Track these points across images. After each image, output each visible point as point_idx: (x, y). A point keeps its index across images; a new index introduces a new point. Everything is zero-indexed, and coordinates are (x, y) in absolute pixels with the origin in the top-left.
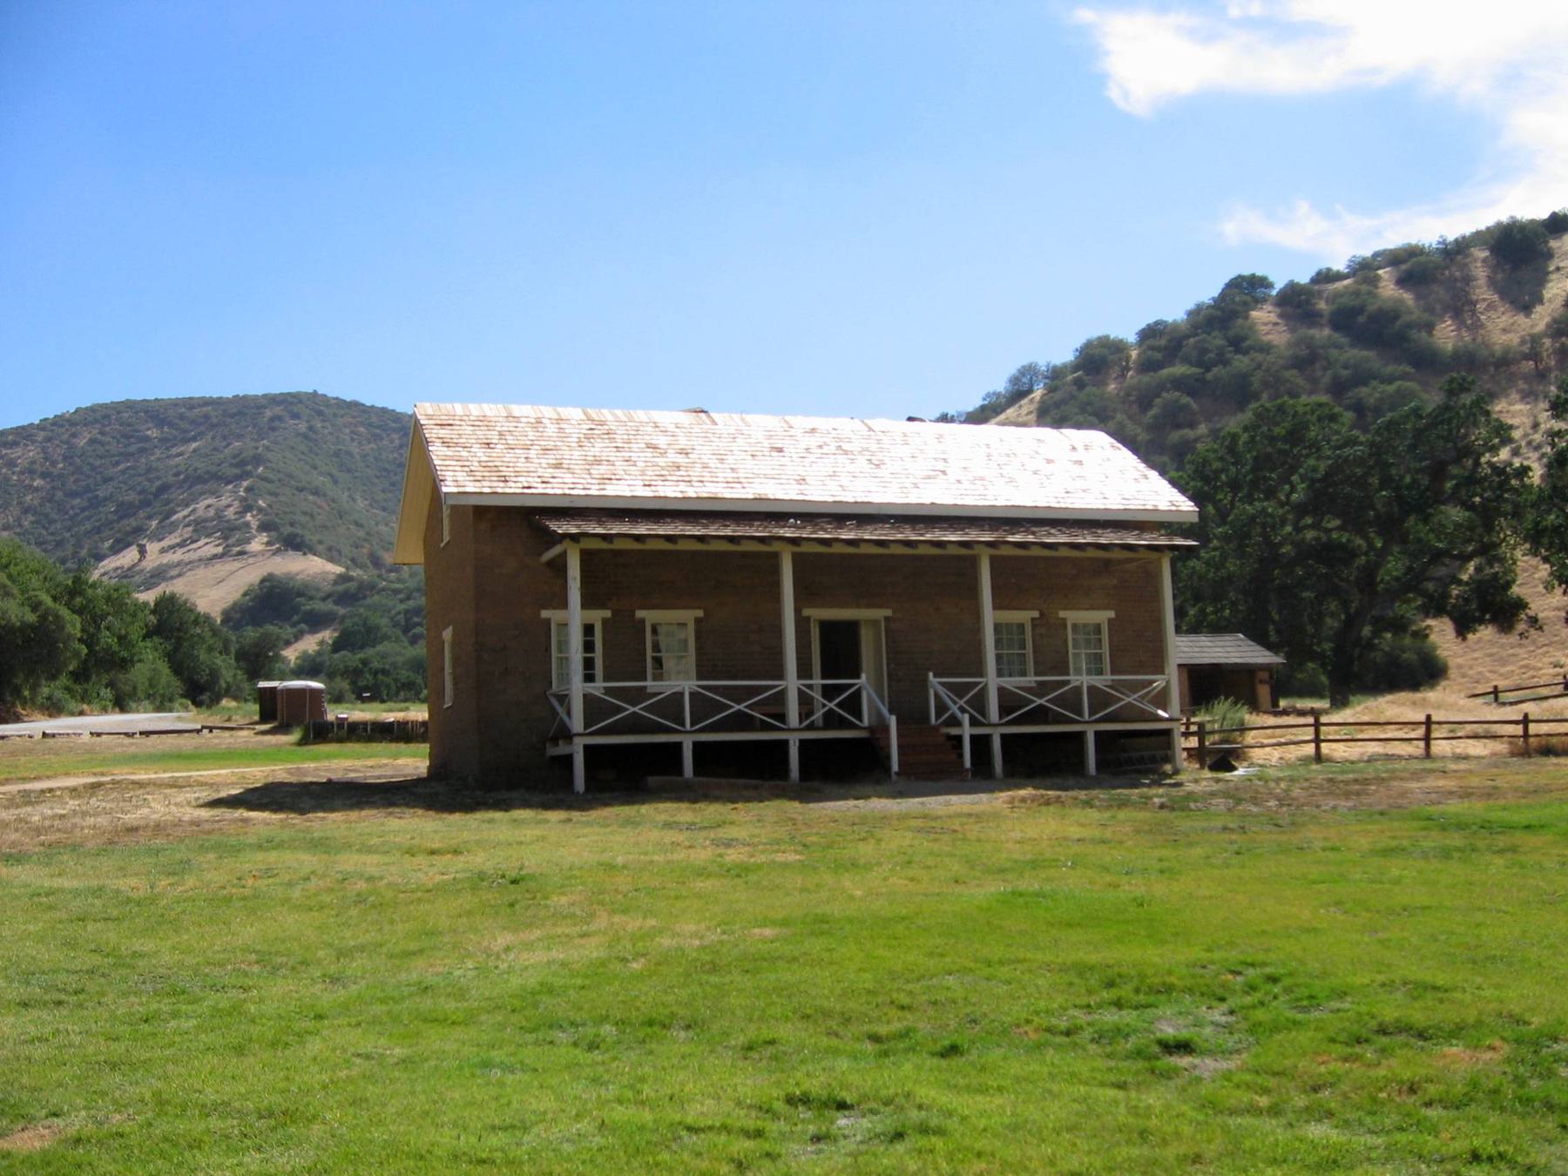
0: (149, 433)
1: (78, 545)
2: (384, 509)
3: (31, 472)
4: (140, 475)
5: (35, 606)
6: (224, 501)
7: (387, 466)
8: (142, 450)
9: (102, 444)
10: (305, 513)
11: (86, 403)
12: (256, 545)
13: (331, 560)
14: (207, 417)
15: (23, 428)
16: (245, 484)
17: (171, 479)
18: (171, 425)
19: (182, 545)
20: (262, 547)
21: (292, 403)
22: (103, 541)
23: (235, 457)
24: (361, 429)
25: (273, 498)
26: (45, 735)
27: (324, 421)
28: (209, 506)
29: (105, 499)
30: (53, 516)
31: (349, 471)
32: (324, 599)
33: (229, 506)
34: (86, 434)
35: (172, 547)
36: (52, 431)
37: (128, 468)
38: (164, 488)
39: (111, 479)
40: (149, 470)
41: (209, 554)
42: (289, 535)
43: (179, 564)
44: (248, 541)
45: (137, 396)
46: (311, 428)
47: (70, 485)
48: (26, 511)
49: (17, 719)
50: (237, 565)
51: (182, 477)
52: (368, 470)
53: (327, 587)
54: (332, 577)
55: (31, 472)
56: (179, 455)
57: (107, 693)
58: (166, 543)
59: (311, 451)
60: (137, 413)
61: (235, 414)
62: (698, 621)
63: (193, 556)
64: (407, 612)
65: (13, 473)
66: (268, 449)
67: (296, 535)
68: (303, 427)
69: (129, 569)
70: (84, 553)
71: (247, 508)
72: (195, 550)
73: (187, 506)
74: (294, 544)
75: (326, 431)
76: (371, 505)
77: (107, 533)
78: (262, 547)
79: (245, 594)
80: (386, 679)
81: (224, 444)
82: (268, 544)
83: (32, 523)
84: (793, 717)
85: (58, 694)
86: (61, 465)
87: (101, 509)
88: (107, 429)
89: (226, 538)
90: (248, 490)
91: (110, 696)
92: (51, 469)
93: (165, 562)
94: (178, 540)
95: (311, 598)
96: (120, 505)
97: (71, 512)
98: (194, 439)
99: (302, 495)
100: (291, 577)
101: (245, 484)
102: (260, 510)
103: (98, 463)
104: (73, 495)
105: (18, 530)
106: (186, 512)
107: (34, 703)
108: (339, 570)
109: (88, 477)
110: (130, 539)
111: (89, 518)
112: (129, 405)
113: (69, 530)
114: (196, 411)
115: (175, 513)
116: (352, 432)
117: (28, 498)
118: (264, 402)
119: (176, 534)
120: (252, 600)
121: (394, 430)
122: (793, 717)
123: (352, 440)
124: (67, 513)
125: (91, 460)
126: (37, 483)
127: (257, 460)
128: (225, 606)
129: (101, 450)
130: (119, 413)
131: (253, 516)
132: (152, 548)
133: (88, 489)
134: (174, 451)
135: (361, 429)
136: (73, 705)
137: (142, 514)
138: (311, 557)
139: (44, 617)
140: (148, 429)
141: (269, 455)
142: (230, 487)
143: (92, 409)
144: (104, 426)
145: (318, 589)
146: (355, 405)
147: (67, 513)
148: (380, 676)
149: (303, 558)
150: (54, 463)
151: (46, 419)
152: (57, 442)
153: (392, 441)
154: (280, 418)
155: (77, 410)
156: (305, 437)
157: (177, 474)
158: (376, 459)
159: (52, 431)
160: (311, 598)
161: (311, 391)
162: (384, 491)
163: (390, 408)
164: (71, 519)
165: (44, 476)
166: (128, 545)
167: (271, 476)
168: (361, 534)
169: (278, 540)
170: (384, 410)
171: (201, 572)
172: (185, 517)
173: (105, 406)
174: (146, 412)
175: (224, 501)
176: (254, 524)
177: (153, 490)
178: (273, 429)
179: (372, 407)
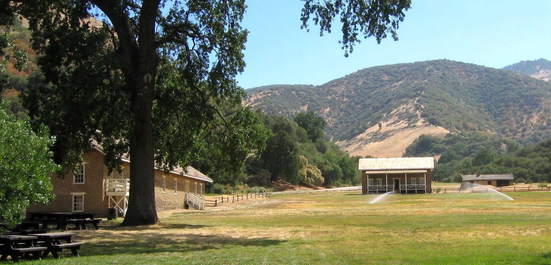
0: (384, 78)
1: (359, 124)
2: (471, 105)
3: (343, 96)
4: (381, 95)
5: (333, 167)
6: (409, 106)
7: (472, 87)
8: (381, 86)
9: (367, 84)
10: (438, 109)
11: (361, 68)
12: (419, 123)
13: (446, 128)
14: (404, 71)
15: (339, 79)
16: (417, 99)
17: (391, 97)
18: (392, 75)
19: (394, 123)
20: (421, 124)
21: (436, 64)
22: (367, 122)
23: (414, 88)
24: (463, 73)
25: (427, 104)
26: (333, 191)
27: (448, 71)
28: (403, 108)
29: (369, 105)
30: (351, 112)
31: (458, 90)
32: (441, 143)
33: (411, 108)
34: (361, 80)
35: (390, 124)
36: (349, 80)
37: (377, 93)
38: (389, 100)
39: (370, 97)
40: (384, 93)
41: (403, 127)
42: (431, 119)
43: (392, 131)
44: (417, 121)
45: (379, 64)
46: (443, 74)
47: (356, 100)
48: (341, 110)
49: (331, 188)
50: (412, 131)
51: (395, 96)
52: (465, 89)
53: (443, 139)
54: (445, 135)
55: (343, 96)
56: (394, 87)
57: (350, 182)
58: (388, 123)
59: (443, 83)
60: (379, 71)
61: (416, 70)
62: (382, 180)
63: (397, 128)
64: (469, 147)
65: (337, 96)
66: (426, 84)
67: (434, 119)
68: (440, 74)
69: (376, 133)
70: (361, 126)
71: (417, 109)
72: (398, 125)
73: (396, 108)
74: (434, 122)
75: (449, 75)
76: (466, 103)
77: (369, 118)
78: (421, 124)
79: (414, 142)
80: (442, 174)
81: (411, 81)
82: (424, 122)
83: (344, 115)
84: (406, 188)
85: (339, 183)
86: (353, 93)
87: (367, 109)
88: (369, 78)
89: (409, 120)
90: (418, 101)
91: (351, 183)
92: (349, 94)
93: (388, 130)
94: (393, 121)
95: (437, 143)
96: (374, 108)
97: (357, 110)
98: (400, 80)
99: (438, 102)
100: (429, 135)
101: (417, 99)
102: (422, 109)
103: (366, 91)
104: (357, 104)
105: (338, 118)
106: (395, 111)
107: (334, 184)
108: (448, 132)
109: (362, 97)
110: (376, 121)
111: (363, 112)
112: (376, 68)
113: (356, 117)
114: (401, 69)
115: (392, 111)
116: (459, 74)
117: (342, 106)
118: (425, 64)
119: (392, 119)
120: (416, 144)
121: (476, 72)
122: (406, 188)
123: (460, 77)
124: (355, 111)
125: (363, 90)
126: (345, 100)
127: (422, 89)
128: (407, 146)
129: (367, 86)
130: (373, 71)
131: (419, 112)
132: (384, 124)
133: (362, 101)
134: (393, 85)
135: (463, 73)
136: (342, 185)
137: (381, 111)
138: (438, 127)
139: (335, 169)
140: (384, 77)
141: (426, 86)
142: (412, 100)
143: (363, 71)
144: (368, 77)
145: (439, 140)
146: (461, 63)
147: (355, 111)
148: (440, 174)
149: (436, 128)
150: (351, 92)
151: (347, 76)
152: (351, 84)
153: (475, 77)
154: (432, 71)
155: (358, 71)
156: (441, 78)
157: (393, 95)
158: (468, 84)
159: (349, 80)
160: (437, 143)
161: (443, 59)
162: (471, 97)
163: (474, 63)
164: (357, 112)
165: (347, 97)
166: (376, 123)
167: (427, 95)
168: (460, 116)
169: (427, 121)
170: (472, 65)
171: (400, 134)
172: (395, 112)
173: (368, 69)
174: (383, 70)
175: (409, 106)
176: (419, 115)
177: (385, 101)
178: (429, 75)
179: (467, 64)
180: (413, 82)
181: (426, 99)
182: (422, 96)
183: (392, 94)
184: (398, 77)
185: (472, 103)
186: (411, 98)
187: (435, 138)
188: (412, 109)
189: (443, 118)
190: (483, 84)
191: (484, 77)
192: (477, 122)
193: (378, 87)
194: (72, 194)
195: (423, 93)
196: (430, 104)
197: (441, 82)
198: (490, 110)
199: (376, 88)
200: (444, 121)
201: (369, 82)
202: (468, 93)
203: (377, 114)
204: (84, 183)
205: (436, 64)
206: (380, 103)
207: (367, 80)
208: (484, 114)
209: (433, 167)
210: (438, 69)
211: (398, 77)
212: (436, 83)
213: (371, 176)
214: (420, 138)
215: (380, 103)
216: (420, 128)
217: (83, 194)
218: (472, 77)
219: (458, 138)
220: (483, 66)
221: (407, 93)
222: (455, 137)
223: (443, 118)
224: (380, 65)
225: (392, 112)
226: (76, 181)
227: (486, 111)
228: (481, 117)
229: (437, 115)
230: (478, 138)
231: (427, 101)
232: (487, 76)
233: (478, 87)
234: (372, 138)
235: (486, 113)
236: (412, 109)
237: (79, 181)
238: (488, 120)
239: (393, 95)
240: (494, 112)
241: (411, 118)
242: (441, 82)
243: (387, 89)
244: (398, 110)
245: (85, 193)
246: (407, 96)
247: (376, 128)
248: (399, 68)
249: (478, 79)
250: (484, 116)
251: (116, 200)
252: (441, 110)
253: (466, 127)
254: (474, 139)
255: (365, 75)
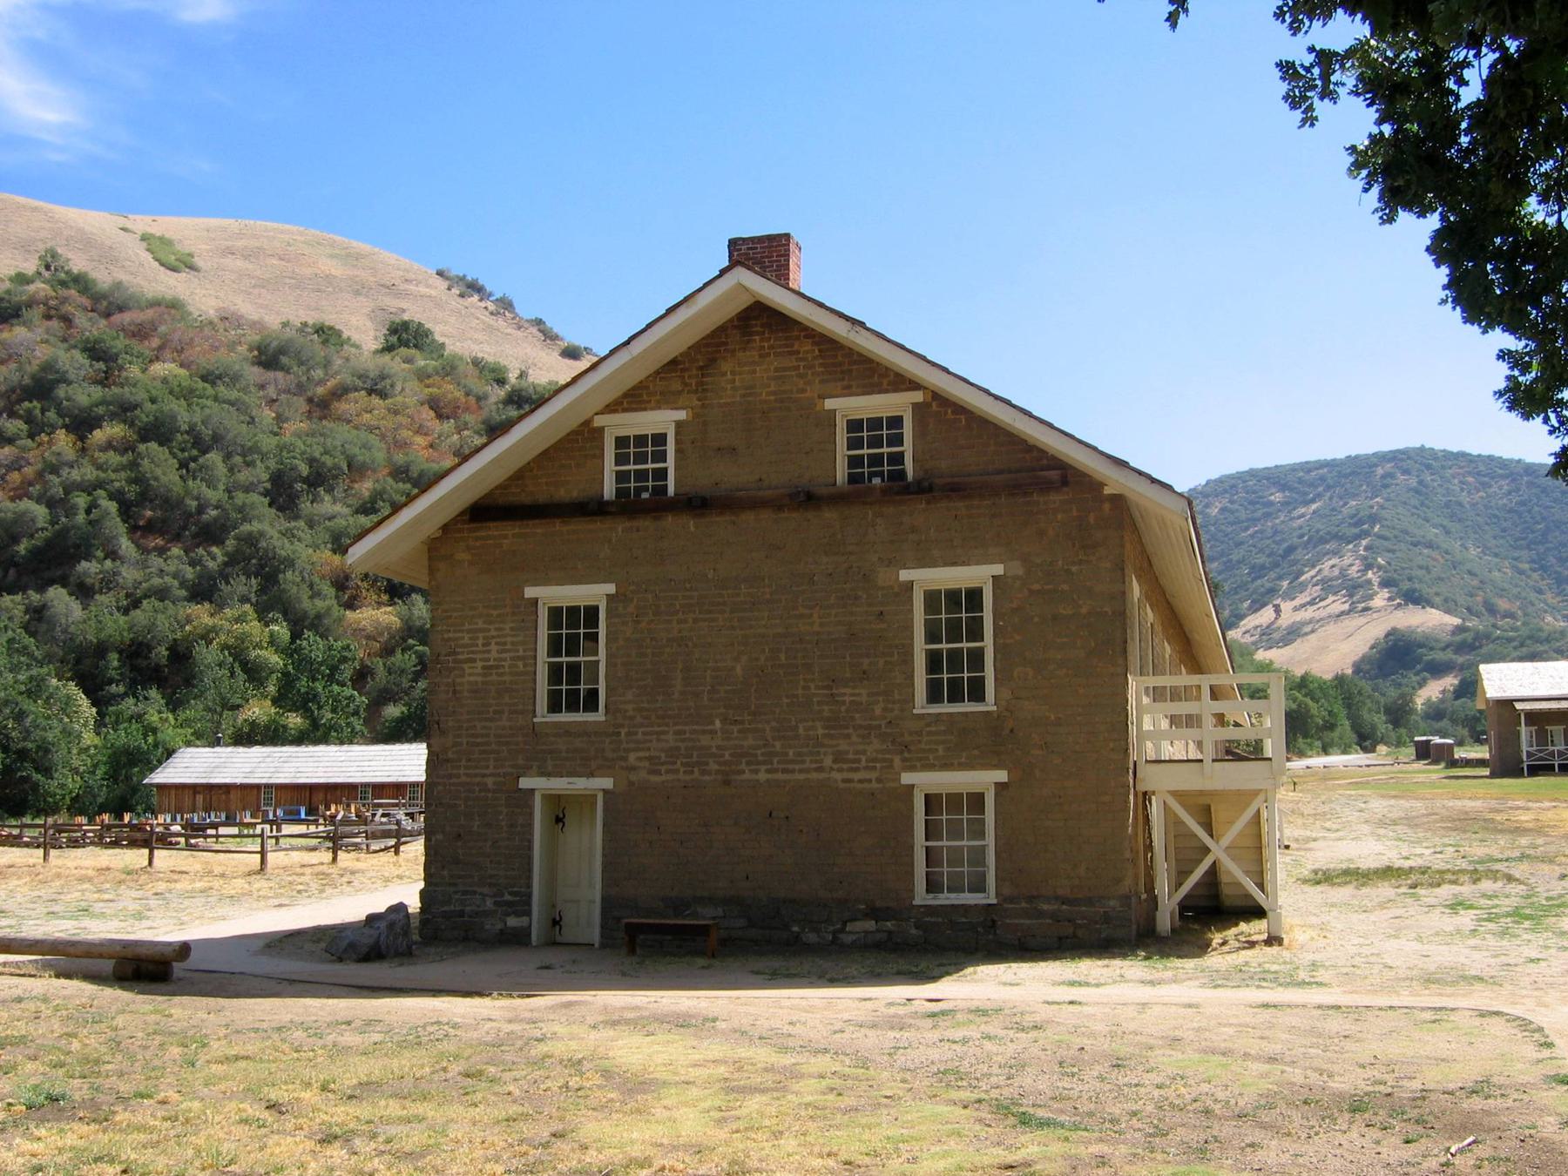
2: (1496, 555)
6: (1347, 561)
7: (1496, 512)
8: (1267, 515)
9: (1232, 512)
10: (1421, 567)
11: (1215, 476)
12: (1379, 601)
13: (1448, 612)
14: (1322, 479)
16: (1364, 543)
18: (1291, 489)
19: (1312, 603)
20: (1384, 603)
21: (1402, 460)
23: (1352, 518)
24: (1470, 479)
25: (1390, 555)
27: (1432, 474)
28: (1333, 566)
29: (1239, 562)
32: (1444, 649)
33: (1351, 565)
35: (1303, 606)
37: (1256, 532)
38: (1291, 549)
39: (1241, 543)
40: (1276, 532)
42: (1408, 590)
43: (1311, 621)
44: (1371, 597)
46: (1421, 482)
50: (1363, 620)
54: (1450, 628)
58: (1297, 602)
59: (1422, 504)
61: (1350, 474)
63: (1323, 613)
66: (1382, 507)
67: (1414, 591)
68: (1413, 482)
69: (1268, 627)
71: (1369, 567)
73: (1313, 566)
74: (1413, 598)
76: (1483, 552)
78: (1384, 603)
79: (1372, 647)
82: (1390, 599)
89: (1351, 596)
90: (1367, 548)
95: (1432, 649)
96: (1253, 567)
98: (1313, 501)
99: (1416, 550)
101: (1364, 543)
102: (1380, 567)
103: (1230, 530)
106: (1313, 573)
108: (1457, 621)
112: (1252, 473)
115: (1303, 574)
116: (1461, 482)
119: (1306, 593)
120: (1379, 652)
121: (1502, 477)
123: (1462, 490)
127: (1373, 519)
128: (1356, 657)
129: (1231, 518)
132: (1286, 606)
133: (1222, 554)
134: (1296, 513)
135: (1470, 479)
137: (1273, 575)
138: (1428, 609)
139: (1299, 706)
142: (1351, 546)
143: (1220, 481)
145: (1437, 641)
146: (1463, 455)
153: (1500, 488)
154: (1391, 475)
155: (1208, 482)
157: (1301, 536)
160: (1432, 649)
161: (1418, 445)
162: (1495, 538)
170: (1491, 458)
171: (1331, 628)
172: (1312, 577)
174: (1268, 479)
177: (1281, 552)
178: (1386, 486)
179: (1479, 456)
180: (1346, 504)
181: (1386, 543)
182: (1375, 535)
183: (1295, 534)
184: (1306, 494)
185: (1497, 550)
186: (1349, 542)
187: (1427, 637)
188: (1355, 568)
189: (1435, 589)
190: (1523, 503)
191: (1524, 488)
192: (1517, 597)
193: (1259, 520)
194: (907, 778)
195: (1376, 529)
196: (1398, 554)
197: (1417, 503)
198: (1543, 568)
199: (1255, 521)
200: (1437, 594)
201: (1236, 506)
202: (1487, 527)
203: (1264, 583)
204: (989, 705)
205: (1398, 458)
206: (1269, 556)
207: (1232, 502)
208: (1529, 577)
209: (423, 778)
210: (1406, 472)
211: (1306, 494)
212: (1405, 503)
213: (1532, 717)
214: (1388, 635)
215: (1269, 556)
216: (1383, 613)
217: (985, 779)
218: (1494, 489)
219: (1487, 636)
220: (1519, 461)
221: (1336, 529)
222: (1477, 633)
223: (1435, 589)
224: (1260, 465)
225: (1303, 578)
226: (934, 695)
227: (1534, 570)
228: (1523, 584)
229: (1421, 581)
230: (1540, 634)
231: (1391, 547)
232: (1530, 484)
233: (1511, 511)
234: (1261, 641)
235: (1535, 576)
236: (1355, 568)
237: (955, 697)
238: (1540, 592)
239: (1301, 536)
240: (1556, 572)
241: (1354, 590)
242: (1417, 503)
243: (1283, 522)
244: (1320, 570)
245: (1002, 776)
246: (1335, 536)
247: (1266, 615)
248: (1309, 471)
249: (1509, 493)
250: (1532, 583)
251: (1209, 828)
252: (1428, 569)
253: (1492, 610)
254: (1530, 637)
255: (1225, 491)
